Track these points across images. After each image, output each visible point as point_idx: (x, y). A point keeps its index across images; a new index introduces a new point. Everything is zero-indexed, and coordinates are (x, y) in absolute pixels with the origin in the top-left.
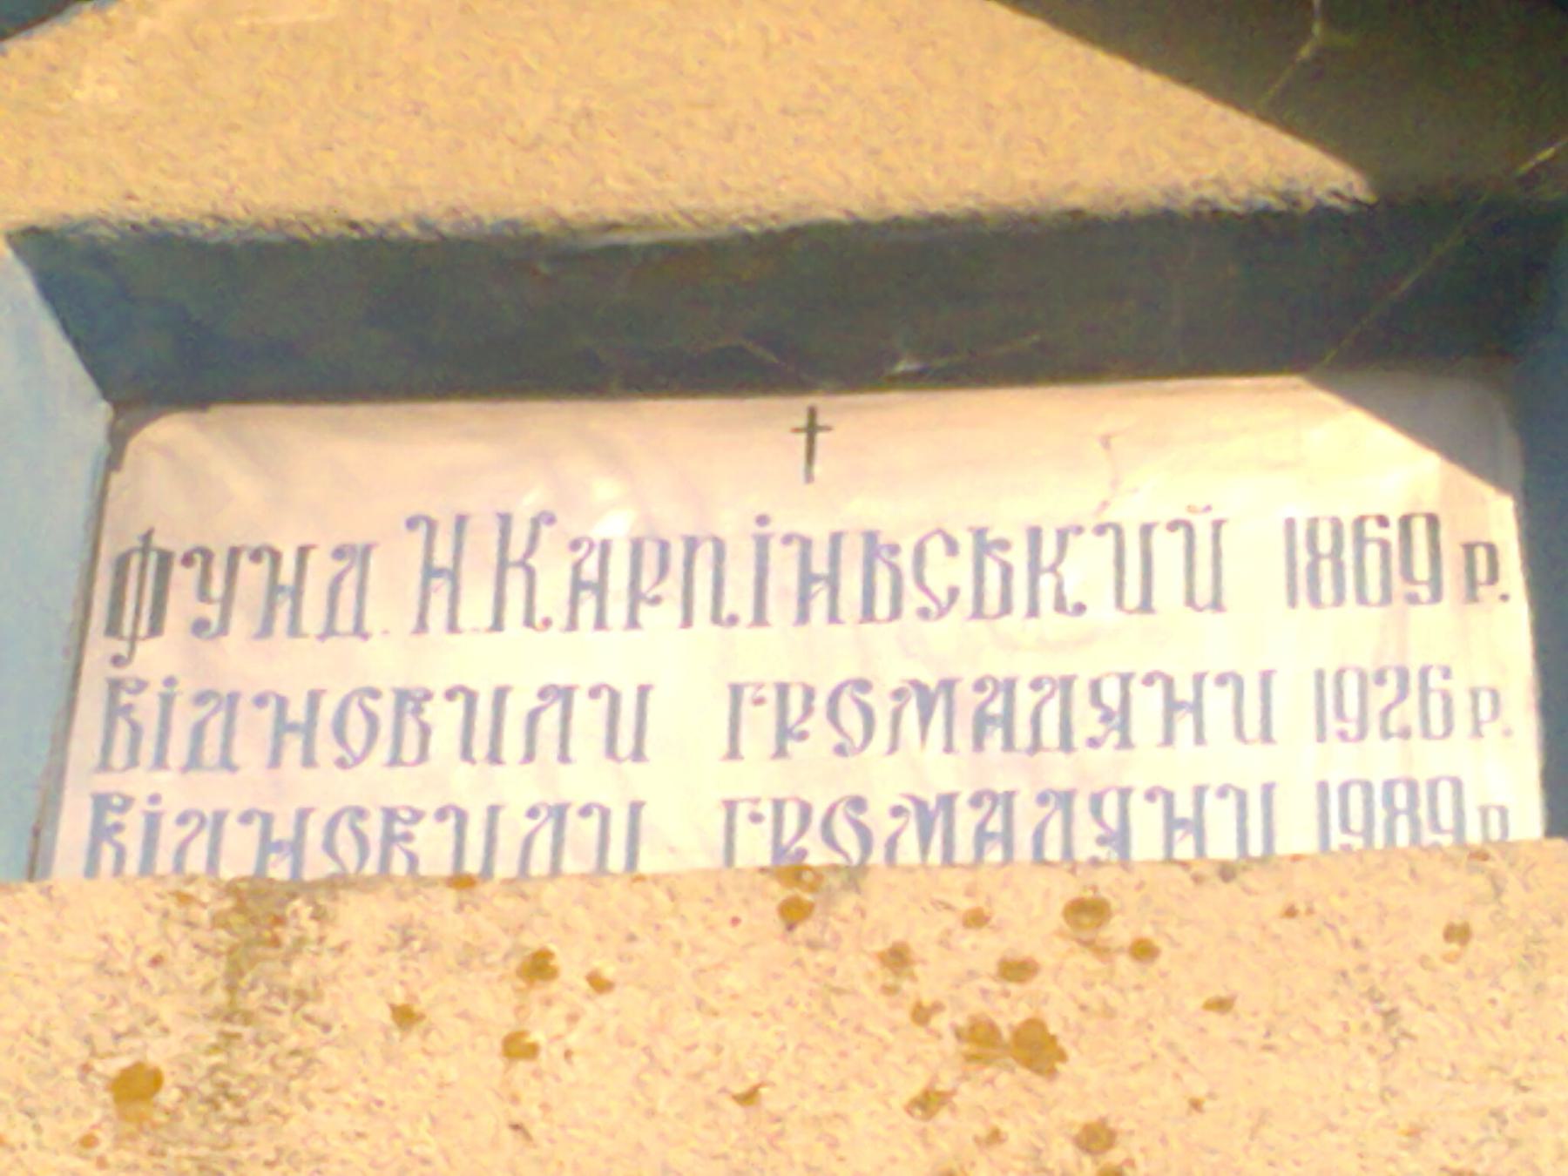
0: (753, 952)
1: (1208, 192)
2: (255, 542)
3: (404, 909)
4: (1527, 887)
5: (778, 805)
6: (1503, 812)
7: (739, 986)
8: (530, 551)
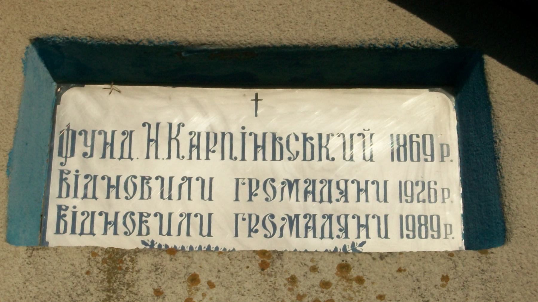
0: (253, 276)
1: (373, 42)
2: (99, 129)
3: (156, 259)
4: (464, 266)
5: (250, 216)
6: (451, 226)
7: (250, 287)
8: (178, 135)
